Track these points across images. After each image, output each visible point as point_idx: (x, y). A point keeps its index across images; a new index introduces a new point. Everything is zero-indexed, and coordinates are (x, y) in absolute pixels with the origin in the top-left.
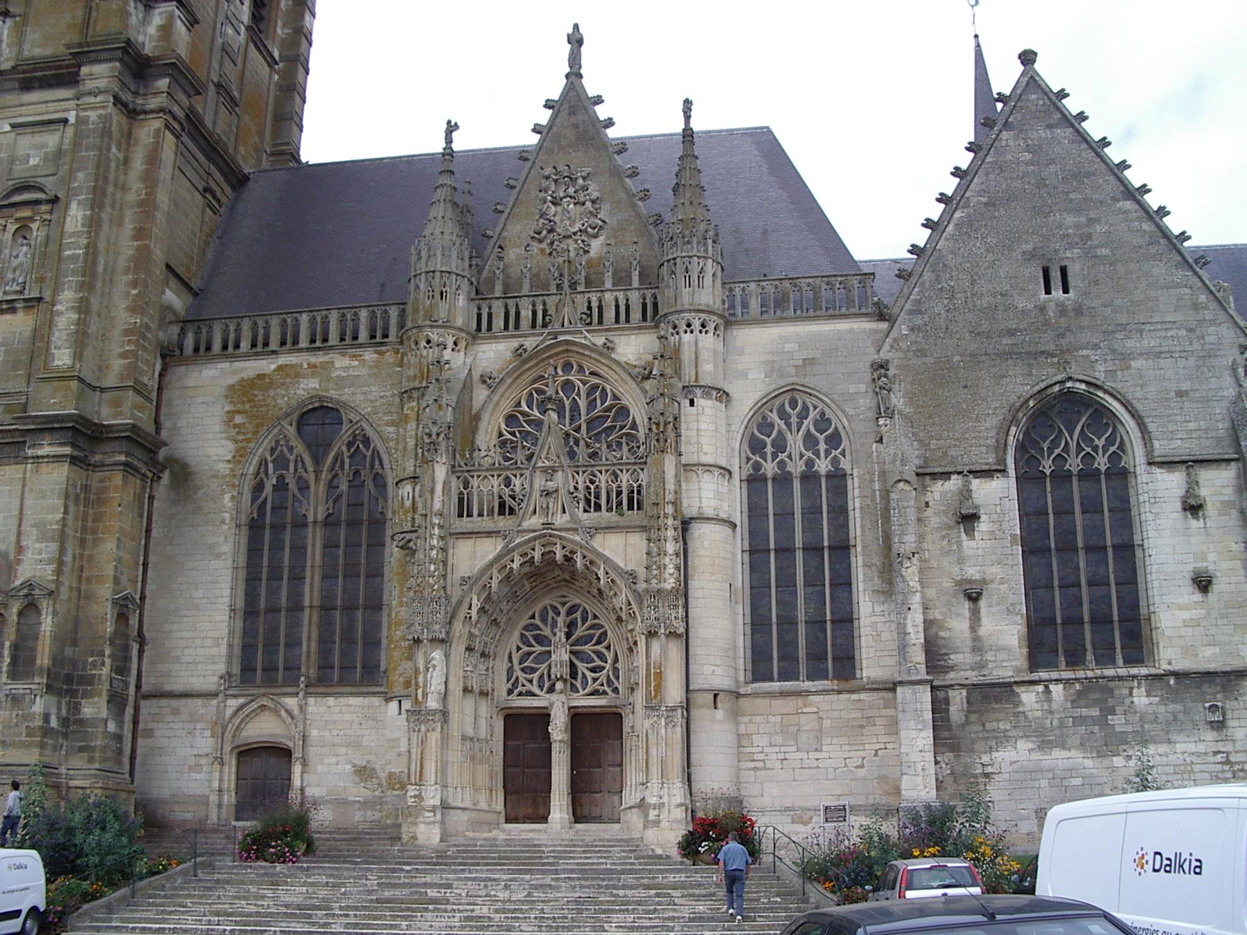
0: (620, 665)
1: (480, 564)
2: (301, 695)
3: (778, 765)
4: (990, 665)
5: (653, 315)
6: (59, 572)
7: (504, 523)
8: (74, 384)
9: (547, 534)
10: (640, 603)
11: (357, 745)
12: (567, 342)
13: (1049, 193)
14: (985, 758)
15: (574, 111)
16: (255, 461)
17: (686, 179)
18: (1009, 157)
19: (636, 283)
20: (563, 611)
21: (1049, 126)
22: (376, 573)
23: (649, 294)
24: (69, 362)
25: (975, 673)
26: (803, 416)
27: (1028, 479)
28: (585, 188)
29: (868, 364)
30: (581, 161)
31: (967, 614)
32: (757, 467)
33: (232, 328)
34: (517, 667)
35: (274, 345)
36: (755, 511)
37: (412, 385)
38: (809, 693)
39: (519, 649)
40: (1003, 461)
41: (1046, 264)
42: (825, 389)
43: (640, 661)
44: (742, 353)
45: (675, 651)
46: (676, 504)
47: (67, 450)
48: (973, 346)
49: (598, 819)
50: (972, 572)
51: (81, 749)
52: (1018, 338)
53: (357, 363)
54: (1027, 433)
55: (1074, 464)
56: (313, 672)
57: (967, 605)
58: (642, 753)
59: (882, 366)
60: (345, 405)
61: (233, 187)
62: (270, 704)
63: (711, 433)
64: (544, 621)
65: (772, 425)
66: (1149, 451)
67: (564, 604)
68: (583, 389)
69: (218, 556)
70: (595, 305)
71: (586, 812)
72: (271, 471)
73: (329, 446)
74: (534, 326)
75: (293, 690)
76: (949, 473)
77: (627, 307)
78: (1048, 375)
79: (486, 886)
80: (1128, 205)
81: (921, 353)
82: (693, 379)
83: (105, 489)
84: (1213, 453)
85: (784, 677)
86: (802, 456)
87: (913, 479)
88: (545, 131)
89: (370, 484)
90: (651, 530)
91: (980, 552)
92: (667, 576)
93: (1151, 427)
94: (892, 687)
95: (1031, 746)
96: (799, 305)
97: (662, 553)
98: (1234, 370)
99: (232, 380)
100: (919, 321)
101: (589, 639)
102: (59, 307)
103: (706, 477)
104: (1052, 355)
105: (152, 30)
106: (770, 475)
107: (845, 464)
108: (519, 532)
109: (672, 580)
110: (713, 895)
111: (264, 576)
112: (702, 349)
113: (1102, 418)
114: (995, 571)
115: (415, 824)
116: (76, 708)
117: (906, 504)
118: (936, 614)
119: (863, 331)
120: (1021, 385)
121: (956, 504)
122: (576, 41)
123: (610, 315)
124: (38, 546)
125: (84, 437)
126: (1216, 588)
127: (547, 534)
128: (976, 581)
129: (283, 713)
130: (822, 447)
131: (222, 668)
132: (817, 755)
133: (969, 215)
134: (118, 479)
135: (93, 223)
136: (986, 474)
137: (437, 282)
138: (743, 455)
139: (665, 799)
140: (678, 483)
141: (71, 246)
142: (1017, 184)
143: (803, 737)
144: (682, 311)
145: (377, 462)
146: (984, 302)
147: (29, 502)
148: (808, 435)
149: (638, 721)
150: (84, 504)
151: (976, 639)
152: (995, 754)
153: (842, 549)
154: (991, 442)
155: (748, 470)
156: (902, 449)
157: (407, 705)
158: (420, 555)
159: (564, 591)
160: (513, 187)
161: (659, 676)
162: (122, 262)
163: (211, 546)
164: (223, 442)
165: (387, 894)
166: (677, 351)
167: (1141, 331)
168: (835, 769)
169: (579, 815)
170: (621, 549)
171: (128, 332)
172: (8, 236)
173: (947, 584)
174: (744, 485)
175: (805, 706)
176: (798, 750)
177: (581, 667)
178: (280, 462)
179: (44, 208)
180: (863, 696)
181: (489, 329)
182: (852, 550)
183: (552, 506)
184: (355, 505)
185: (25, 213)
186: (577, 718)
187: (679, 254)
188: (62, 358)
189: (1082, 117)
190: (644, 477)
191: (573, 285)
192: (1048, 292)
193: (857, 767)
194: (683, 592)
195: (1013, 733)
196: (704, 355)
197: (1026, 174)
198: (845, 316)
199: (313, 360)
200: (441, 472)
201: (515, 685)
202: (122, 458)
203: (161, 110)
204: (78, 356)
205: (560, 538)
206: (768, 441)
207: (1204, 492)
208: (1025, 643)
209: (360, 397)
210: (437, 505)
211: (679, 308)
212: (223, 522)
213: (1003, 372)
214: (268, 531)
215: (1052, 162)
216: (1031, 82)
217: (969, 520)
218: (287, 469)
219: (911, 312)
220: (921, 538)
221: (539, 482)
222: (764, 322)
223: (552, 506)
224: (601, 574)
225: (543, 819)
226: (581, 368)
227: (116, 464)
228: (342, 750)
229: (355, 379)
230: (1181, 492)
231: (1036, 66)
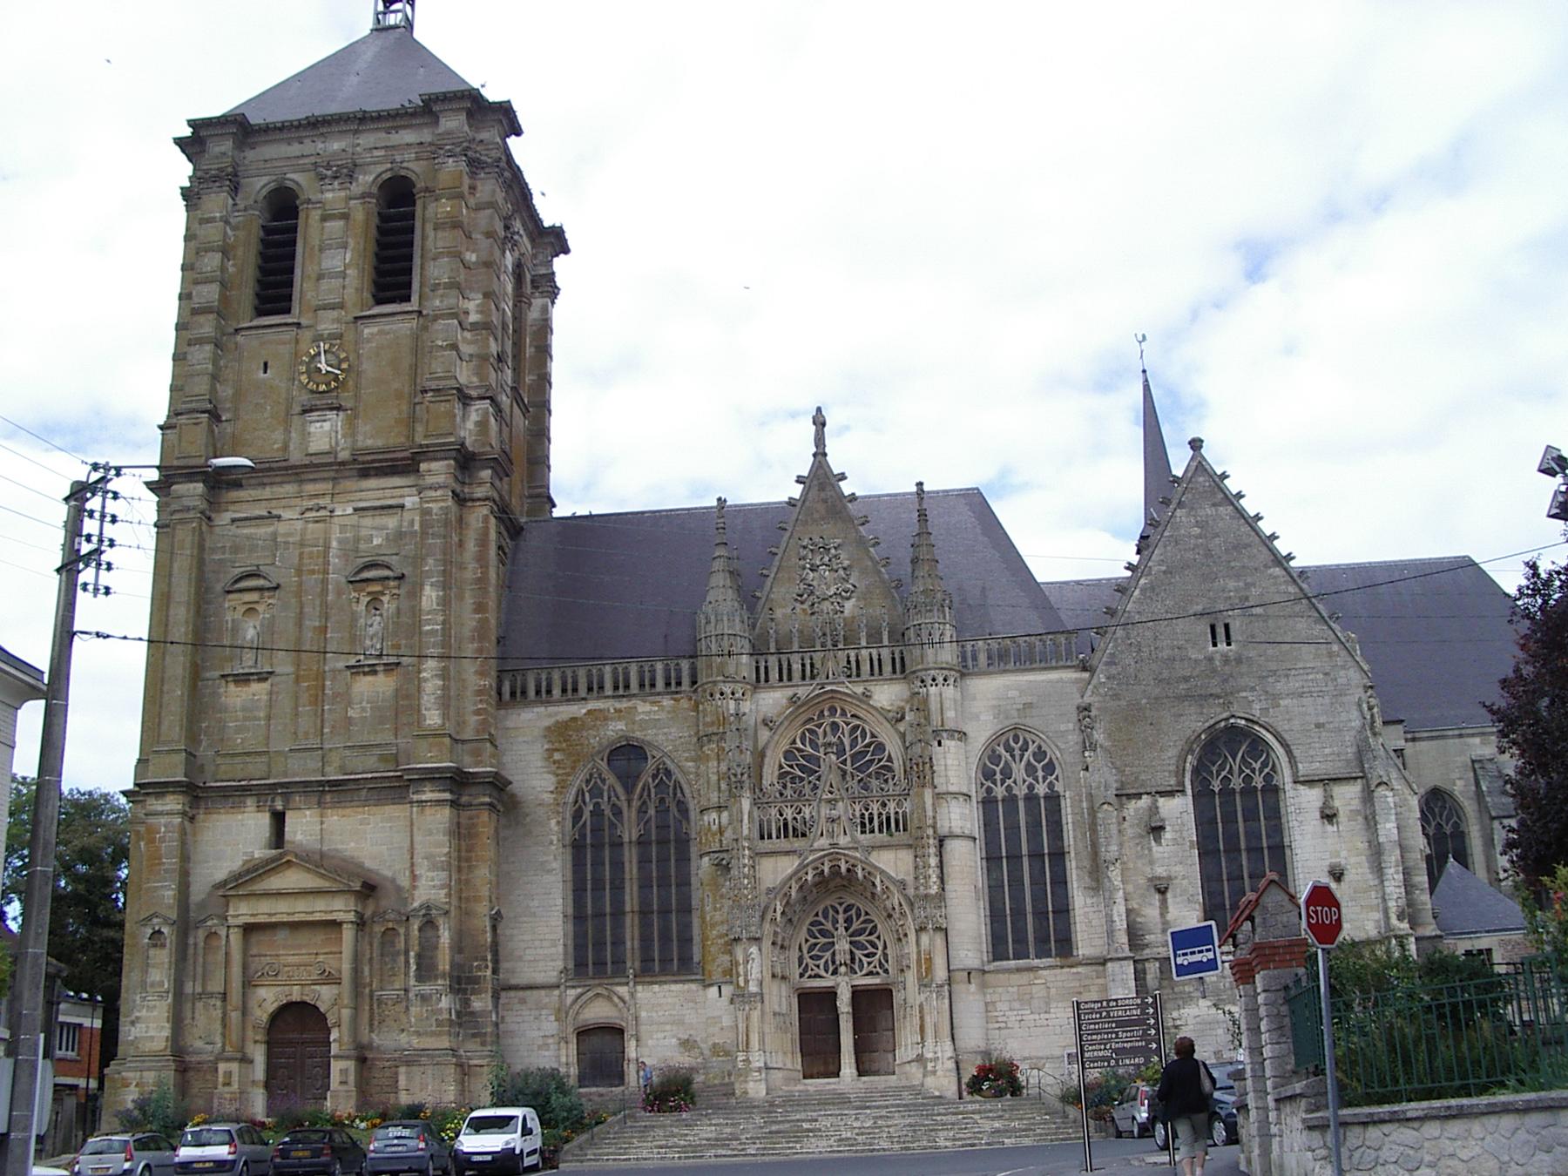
0: (888, 951)
1: (781, 877)
5: (901, 668)
6: (449, 895)
7: (798, 844)
8: (447, 740)
9: (834, 854)
10: (911, 904)
11: (680, 1022)
12: (832, 691)
14: (1175, 1014)
17: (923, 553)
19: (886, 642)
20: (841, 910)
21: (1214, 505)
22: (684, 882)
23: (897, 650)
24: (439, 722)
26: (1024, 749)
27: (1202, 796)
30: (831, 533)
32: (989, 790)
33: (544, 677)
34: (806, 956)
35: (582, 692)
36: (989, 824)
37: (710, 730)
43: (911, 948)
44: (974, 699)
45: (939, 939)
46: (934, 827)
47: (447, 796)
48: (1157, 691)
49: (876, 1073)
50: (1160, 871)
51: (474, 1036)
54: (1200, 760)
55: (1237, 783)
56: (637, 964)
57: (1157, 896)
58: (917, 1021)
59: (1085, 709)
60: (649, 744)
61: (512, 539)
62: (605, 993)
63: (956, 766)
64: (826, 917)
66: (1295, 773)
68: (847, 729)
69: (549, 871)
70: (853, 659)
71: (867, 1066)
74: (803, 678)
78: (1216, 714)
80: (1277, 571)
81: (1116, 697)
83: (474, 825)
84: (1343, 772)
87: (1113, 800)
89: (674, 809)
90: (916, 846)
93: (1296, 753)
94: (1103, 962)
96: (1018, 659)
97: (927, 866)
98: (1360, 706)
101: (864, 933)
102: (424, 674)
103: (954, 803)
105: (470, 425)
107: (1059, 787)
112: (944, 696)
113: (1258, 747)
114: (1178, 870)
116: (466, 1003)
118: (1134, 904)
120: (1195, 722)
121: (1146, 818)
122: (820, 422)
123: (866, 667)
124: (430, 874)
125: (457, 781)
126: (1346, 878)
127: (834, 854)
129: (616, 999)
130: (1040, 774)
131: (560, 964)
134: (485, 816)
135: (445, 602)
136: (1170, 794)
137: (726, 644)
140: (935, 811)
141: (428, 622)
142: (1190, 555)
143: (1035, 1003)
146: (1165, 654)
147: (417, 838)
149: (909, 993)
150: (461, 834)
153: (1059, 856)
154: (1173, 768)
155: (982, 793)
156: (1103, 777)
158: (734, 872)
161: (929, 960)
162: (467, 632)
163: (543, 863)
165: (774, 1128)
166: (926, 700)
167: (1287, 676)
169: (861, 1072)
170: (893, 863)
171: (479, 692)
172: (362, 607)
173: (1142, 881)
177: (858, 953)
178: (596, 792)
179: (392, 583)
180: (1080, 969)
181: (767, 681)
183: (834, 829)
184: (663, 827)
185: (376, 588)
186: (858, 994)
188: (433, 718)
189: (1240, 496)
190: (907, 806)
192: (1215, 645)
194: (941, 895)
196: (947, 704)
197: (1196, 546)
198: (1056, 668)
199: (618, 706)
200: (746, 804)
201: (806, 970)
202: (487, 799)
203: (487, 499)
204: (445, 716)
206: (998, 769)
207: (1337, 803)
210: (746, 832)
212: (551, 843)
214: (590, 849)
216: (1199, 466)
217: (1157, 830)
219: (1107, 664)
220: (1121, 845)
221: (825, 811)
222: (991, 673)
223: (834, 829)
224: (878, 882)
226: (844, 714)
227: (483, 804)
228: (668, 1027)
229: (656, 720)
230: (1320, 804)
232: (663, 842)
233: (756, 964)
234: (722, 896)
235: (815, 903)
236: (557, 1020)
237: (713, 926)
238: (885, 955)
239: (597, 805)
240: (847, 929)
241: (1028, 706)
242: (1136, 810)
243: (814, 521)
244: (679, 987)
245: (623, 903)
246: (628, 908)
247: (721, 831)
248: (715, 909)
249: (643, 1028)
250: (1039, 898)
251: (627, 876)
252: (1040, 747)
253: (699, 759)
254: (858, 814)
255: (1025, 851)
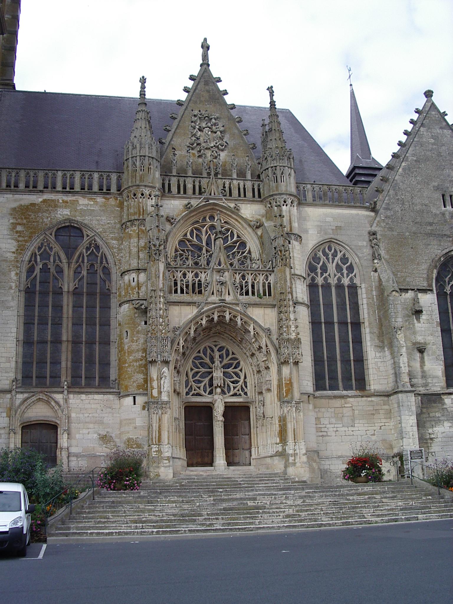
0: (248, 380)
2: (66, 392)
3: (333, 434)
4: (430, 385)
5: (258, 196)
7: (196, 298)
9: (222, 306)
12: (214, 204)
13: (443, 160)
14: (430, 431)
15: (205, 84)
16: (29, 253)
18: (424, 140)
22: (106, 324)
23: (256, 183)
25: (423, 388)
26: (335, 255)
27: (441, 295)
28: (215, 124)
29: (367, 232)
31: (419, 360)
38: (348, 397)
39: (192, 370)
40: (431, 286)
41: (444, 193)
42: (347, 243)
48: (414, 229)
50: (420, 339)
52: (434, 227)
53: (92, 203)
56: (69, 379)
57: (418, 355)
63: (299, 256)
64: (205, 354)
65: (319, 259)
67: (216, 346)
69: (8, 308)
70: (227, 186)
72: (38, 260)
73: (76, 248)
75: (60, 390)
76: (408, 290)
77: (244, 189)
79: (275, 498)
81: (391, 229)
82: (289, 230)
85: (332, 388)
86: (335, 276)
88: (192, 91)
89: (100, 272)
91: (423, 329)
92: (292, 332)
95: (450, 425)
96: (332, 199)
99: (15, 205)
100: (389, 213)
104: (450, 237)
106: (320, 284)
107: (357, 281)
108: (206, 303)
109: (294, 334)
110: (395, 497)
111: (36, 322)
114: (430, 339)
115: (158, 467)
117: (397, 303)
119: (363, 215)
121: (411, 305)
122: (205, 47)
123: (235, 192)
127: (222, 306)
128: (422, 343)
129: (53, 403)
130: (345, 272)
131: (12, 375)
132: (353, 429)
133: (408, 165)
137: (146, 162)
138: (307, 273)
139: (298, 451)
142: (429, 153)
143: (345, 420)
144: (283, 194)
145: (104, 260)
146: (418, 208)
148: (337, 265)
151: (423, 372)
152: (435, 429)
153: (357, 325)
157: (140, 400)
159: (216, 339)
160: (175, 118)
164: (10, 241)
168: (361, 436)
169: (230, 463)
170: (264, 317)
174: (308, 287)
175: (346, 403)
176: (343, 426)
180: (373, 399)
182: (362, 325)
184: (92, 284)
186: (229, 409)
187: (278, 164)
191: (216, 174)
193: (371, 435)
195: (442, 418)
205: (229, 308)
208: (444, 375)
209: (95, 222)
211: (280, 192)
212: (11, 288)
213: (428, 243)
215: (443, 145)
217: (418, 313)
218: (49, 260)
221: (217, 277)
223: (221, 290)
225: (211, 463)
228: (91, 426)
229: (93, 212)
231: (432, 98)
232: (91, 294)
233: (165, 382)
234: (138, 332)
235: (199, 343)
236: (9, 416)
237: (130, 353)
238: (245, 383)
239: (45, 265)
240: (221, 362)
241: (338, 228)
242: (405, 299)
243: (201, 102)
244: (100, 397)
245: (61, 334)
246: (64, 338)
247: (139, 286)
248: (132, 341)
249: (73, 425)
250: (345, 351)
251: (65, 316)
252: (344, 255)
253: (120, 240)
254: (238, 281)
255: (336, 320)
